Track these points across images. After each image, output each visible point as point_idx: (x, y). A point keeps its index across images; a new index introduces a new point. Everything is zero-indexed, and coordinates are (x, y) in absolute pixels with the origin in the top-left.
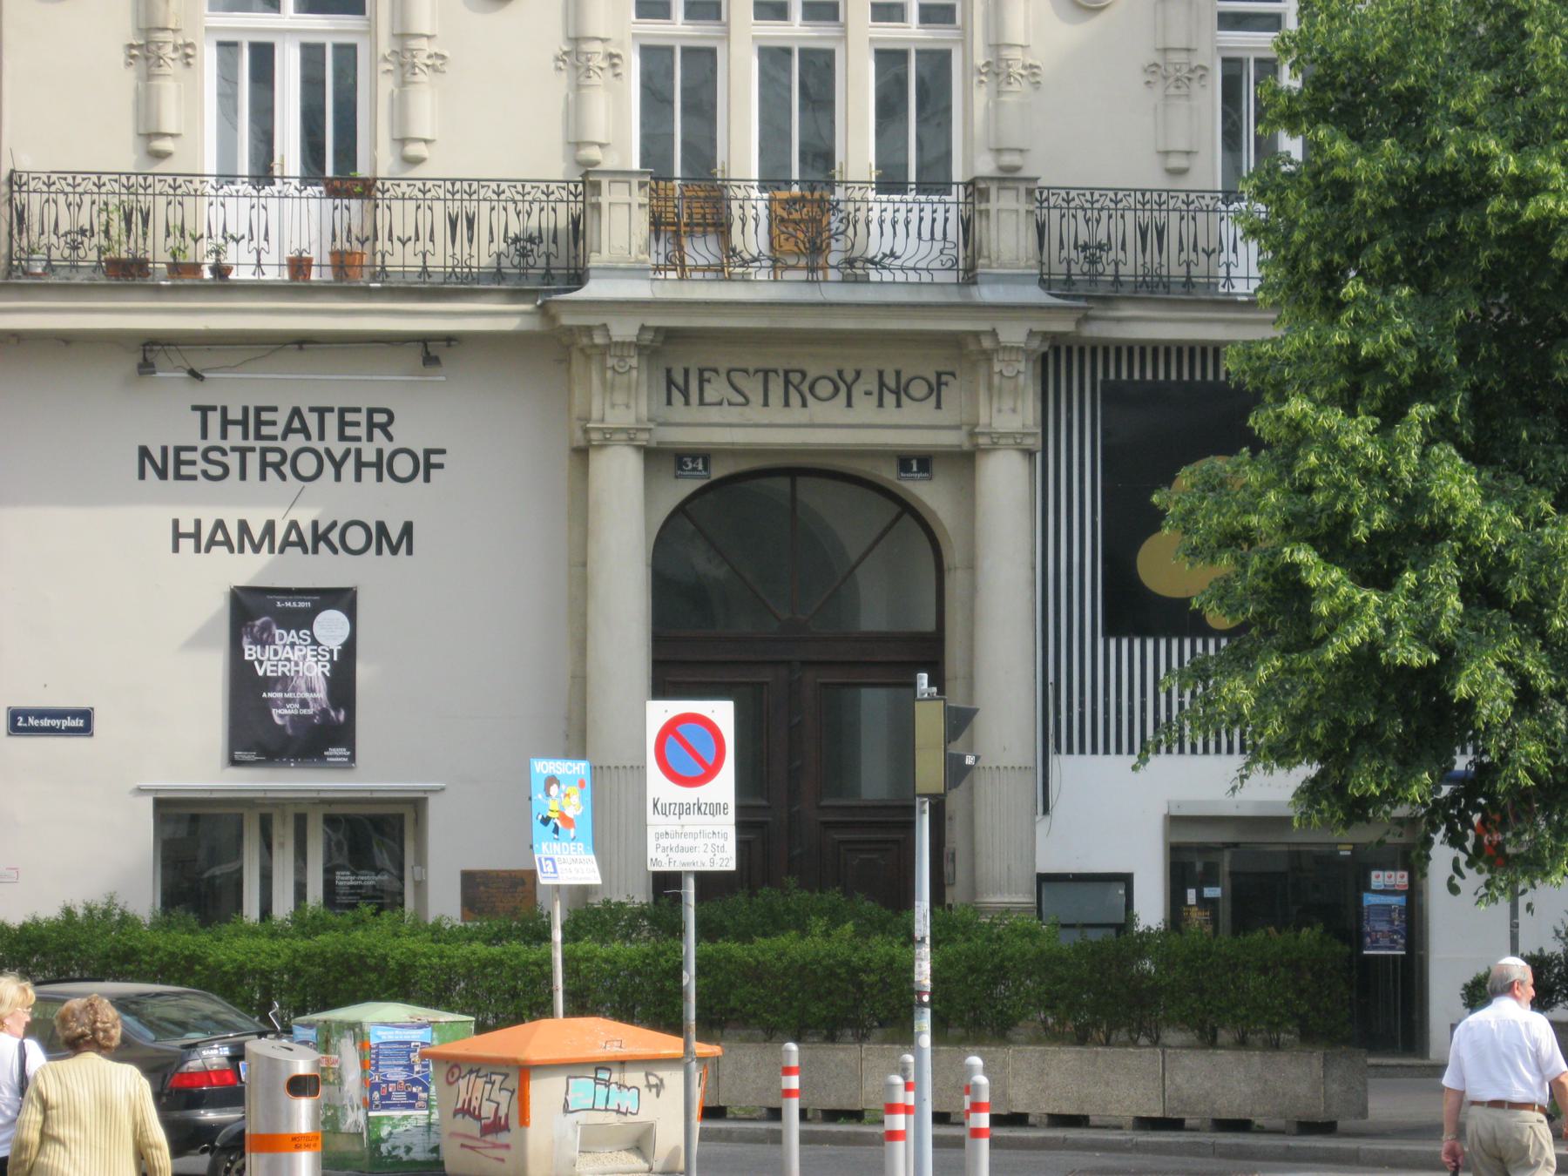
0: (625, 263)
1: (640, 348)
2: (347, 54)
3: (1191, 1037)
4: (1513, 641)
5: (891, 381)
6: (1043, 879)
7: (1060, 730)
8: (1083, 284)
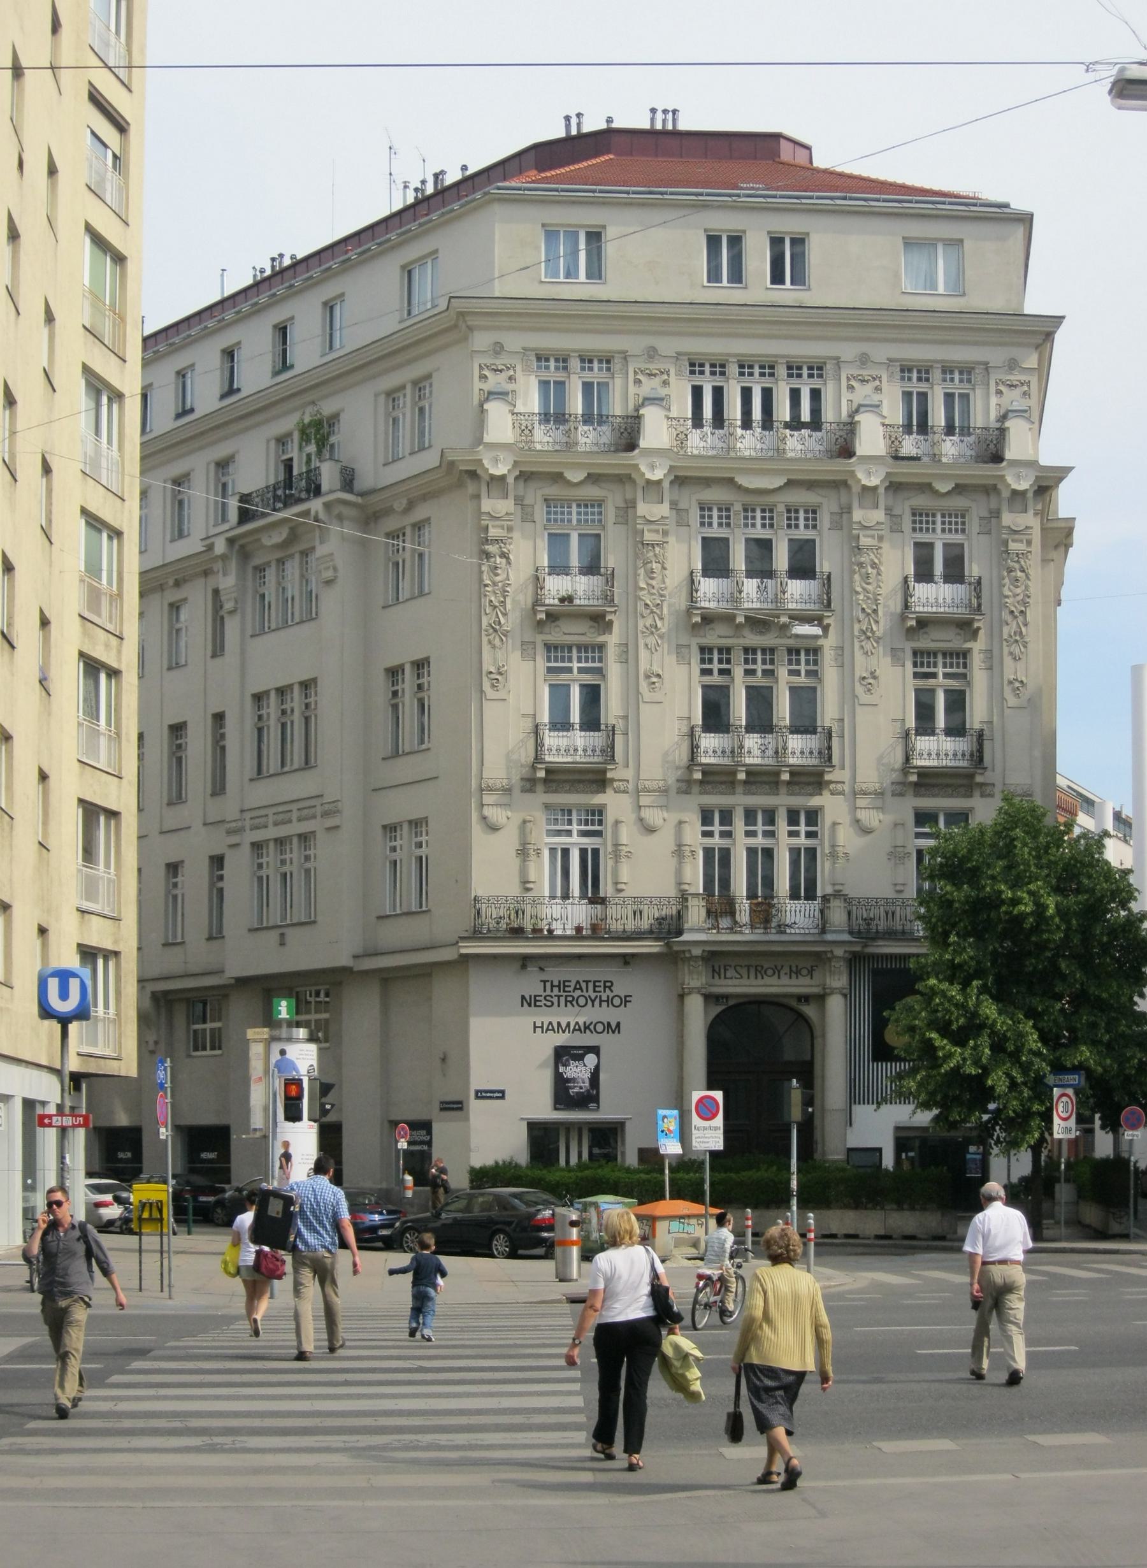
0: (698, 928)
1: (703, 958)
2: (596, 852)
3: (895, 1207)
4: (1008, 1065)
5: (794, 969)
6: (850, 1150)
7: (855, 1096)
8: (865, 933)
